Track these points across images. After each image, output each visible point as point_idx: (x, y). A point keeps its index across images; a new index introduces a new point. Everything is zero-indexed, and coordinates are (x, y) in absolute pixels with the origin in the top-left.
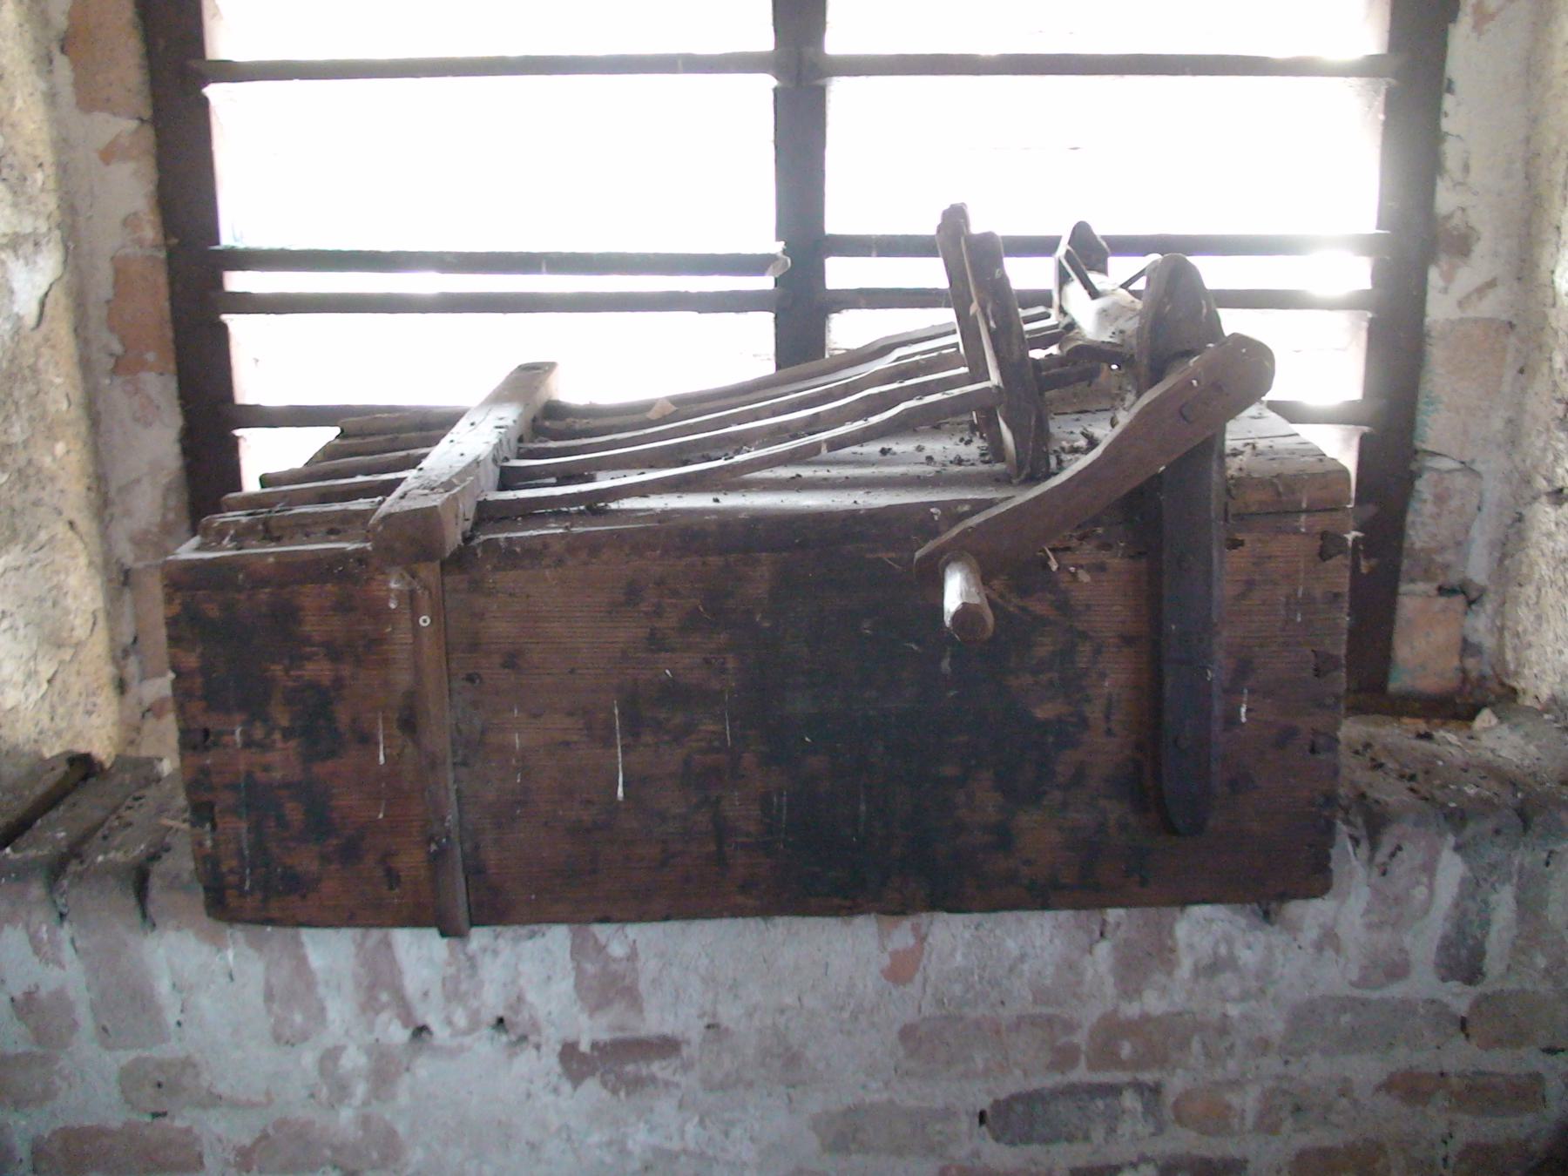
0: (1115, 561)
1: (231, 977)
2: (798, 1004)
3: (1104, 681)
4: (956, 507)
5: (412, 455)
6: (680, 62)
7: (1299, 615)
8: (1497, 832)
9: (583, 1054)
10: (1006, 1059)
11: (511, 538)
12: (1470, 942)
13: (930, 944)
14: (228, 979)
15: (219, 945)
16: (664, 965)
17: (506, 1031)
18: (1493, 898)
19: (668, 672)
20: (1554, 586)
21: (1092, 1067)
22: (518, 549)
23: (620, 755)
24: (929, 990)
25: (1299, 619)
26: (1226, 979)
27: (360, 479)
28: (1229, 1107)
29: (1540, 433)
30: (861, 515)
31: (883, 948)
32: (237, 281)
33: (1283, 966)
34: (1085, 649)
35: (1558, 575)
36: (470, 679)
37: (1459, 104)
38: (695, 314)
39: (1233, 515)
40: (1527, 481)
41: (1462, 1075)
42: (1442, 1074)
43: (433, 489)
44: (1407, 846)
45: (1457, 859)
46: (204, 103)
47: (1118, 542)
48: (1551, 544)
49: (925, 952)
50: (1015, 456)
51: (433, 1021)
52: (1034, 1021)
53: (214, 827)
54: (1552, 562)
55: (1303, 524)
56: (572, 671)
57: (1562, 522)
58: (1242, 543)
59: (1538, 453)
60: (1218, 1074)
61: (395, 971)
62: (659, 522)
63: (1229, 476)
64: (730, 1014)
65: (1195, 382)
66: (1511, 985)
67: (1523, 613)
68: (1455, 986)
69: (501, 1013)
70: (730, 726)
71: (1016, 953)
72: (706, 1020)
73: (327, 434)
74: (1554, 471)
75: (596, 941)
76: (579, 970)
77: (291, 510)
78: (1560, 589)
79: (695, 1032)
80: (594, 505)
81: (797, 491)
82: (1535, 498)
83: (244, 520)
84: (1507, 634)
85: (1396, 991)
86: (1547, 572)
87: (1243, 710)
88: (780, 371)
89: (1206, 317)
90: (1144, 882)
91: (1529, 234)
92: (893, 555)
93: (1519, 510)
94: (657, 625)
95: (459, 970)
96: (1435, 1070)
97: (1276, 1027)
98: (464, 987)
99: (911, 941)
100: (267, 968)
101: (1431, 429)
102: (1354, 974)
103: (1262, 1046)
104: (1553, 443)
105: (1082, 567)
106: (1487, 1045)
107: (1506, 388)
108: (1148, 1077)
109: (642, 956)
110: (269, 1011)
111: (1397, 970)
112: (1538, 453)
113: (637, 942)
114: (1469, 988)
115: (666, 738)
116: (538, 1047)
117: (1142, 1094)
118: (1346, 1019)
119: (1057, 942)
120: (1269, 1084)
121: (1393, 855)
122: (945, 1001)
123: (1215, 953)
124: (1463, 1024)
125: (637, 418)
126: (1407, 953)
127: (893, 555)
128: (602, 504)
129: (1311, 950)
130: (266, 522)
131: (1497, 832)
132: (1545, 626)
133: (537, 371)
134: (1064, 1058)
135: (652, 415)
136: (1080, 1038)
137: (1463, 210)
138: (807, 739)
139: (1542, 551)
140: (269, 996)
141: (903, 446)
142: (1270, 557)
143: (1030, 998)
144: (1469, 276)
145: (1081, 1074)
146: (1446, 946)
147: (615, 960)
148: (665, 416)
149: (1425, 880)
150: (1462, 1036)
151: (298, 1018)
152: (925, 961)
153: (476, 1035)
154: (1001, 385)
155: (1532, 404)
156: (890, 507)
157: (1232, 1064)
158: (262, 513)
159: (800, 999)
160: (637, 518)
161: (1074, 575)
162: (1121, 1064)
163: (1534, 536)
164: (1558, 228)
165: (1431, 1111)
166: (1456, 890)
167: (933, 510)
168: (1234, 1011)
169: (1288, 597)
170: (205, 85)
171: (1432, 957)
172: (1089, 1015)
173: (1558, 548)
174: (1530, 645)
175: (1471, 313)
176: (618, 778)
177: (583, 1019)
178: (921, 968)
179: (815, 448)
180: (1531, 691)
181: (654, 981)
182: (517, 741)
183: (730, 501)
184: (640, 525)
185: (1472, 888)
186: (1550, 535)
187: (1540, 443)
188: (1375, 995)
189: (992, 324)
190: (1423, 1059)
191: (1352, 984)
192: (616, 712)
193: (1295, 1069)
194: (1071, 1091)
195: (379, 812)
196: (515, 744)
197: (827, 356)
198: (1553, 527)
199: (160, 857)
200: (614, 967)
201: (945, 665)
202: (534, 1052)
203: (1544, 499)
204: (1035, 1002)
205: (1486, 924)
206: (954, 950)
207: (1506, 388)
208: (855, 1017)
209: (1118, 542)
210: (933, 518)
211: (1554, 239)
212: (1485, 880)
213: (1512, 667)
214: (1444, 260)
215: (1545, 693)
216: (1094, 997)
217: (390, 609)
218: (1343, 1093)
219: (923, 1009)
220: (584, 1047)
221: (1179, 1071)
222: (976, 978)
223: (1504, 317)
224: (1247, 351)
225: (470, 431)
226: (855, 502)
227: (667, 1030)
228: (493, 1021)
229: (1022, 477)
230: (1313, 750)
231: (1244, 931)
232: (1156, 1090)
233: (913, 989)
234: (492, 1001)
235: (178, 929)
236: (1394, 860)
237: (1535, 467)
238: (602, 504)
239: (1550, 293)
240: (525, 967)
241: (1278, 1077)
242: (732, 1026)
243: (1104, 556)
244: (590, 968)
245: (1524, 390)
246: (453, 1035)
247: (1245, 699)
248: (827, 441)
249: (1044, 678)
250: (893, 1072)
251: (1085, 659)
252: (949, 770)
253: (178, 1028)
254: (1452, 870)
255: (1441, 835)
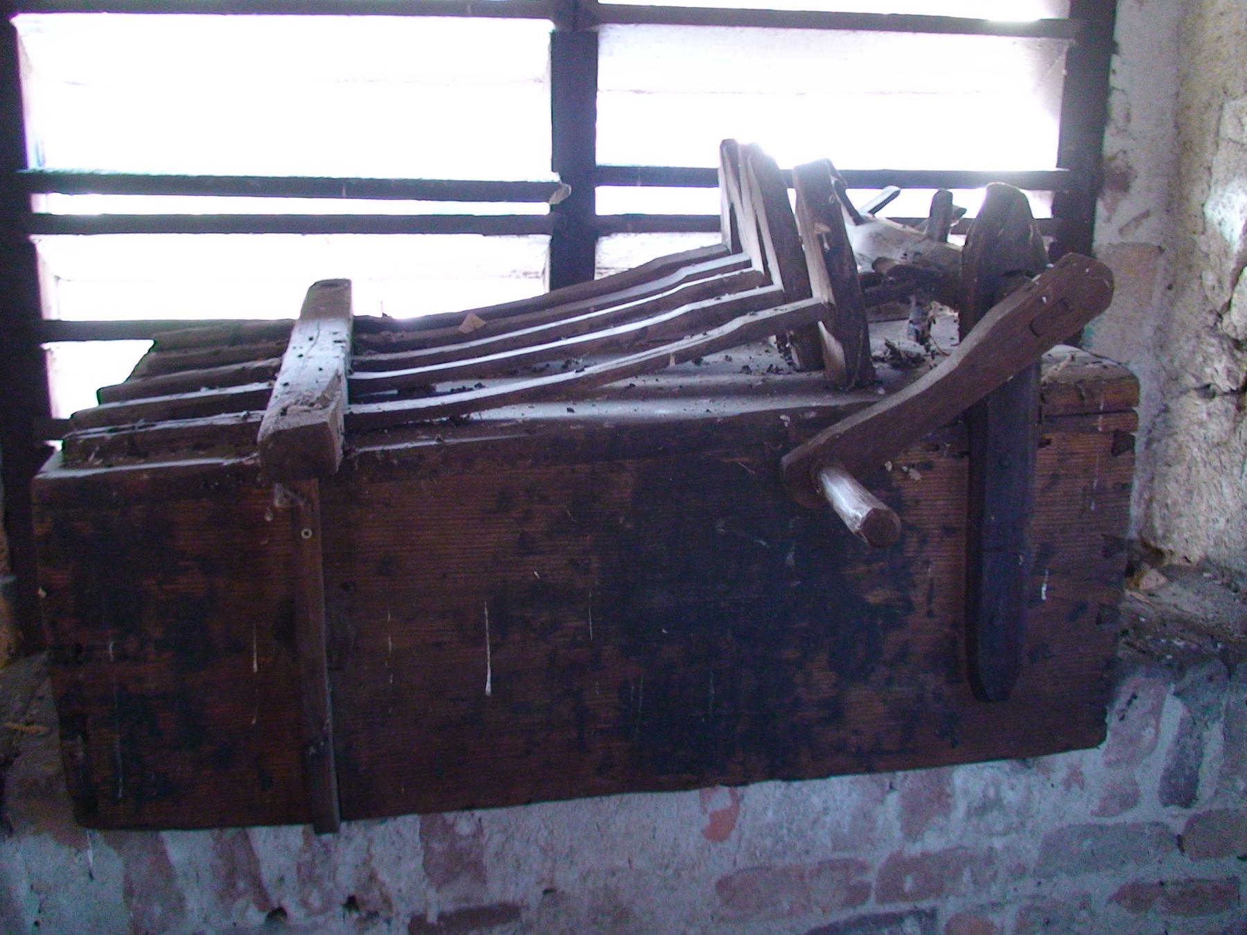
0: (942, 461)
1: (91, 876)
2: (627, 865)
3: (928, 568)
4: (803, 414)
5: (248, 368)
6: (469, 7)
7: (1093, 504)
8: (1210, 679)
9: (432, 925)
10: (809, 900)
11: (388, 451)
12: (1187, 772)
13: (745, 804)
14: (87, 878)
15: (78, 845)
16: (507, 838)
17: (357, 908)
18: (1206, 734)
19: (536, 573)
20: (1208, 466)
21: (881, 900)
22: (395, 462)
23: (489, 653)
24: (743, 845)
25: (1093, 508)
26: (993, 817)
27: (204, 392)
28: (991, 925)
29: (1188, 339)
30: (719, 423)
31: (704, 811)
32: (47, 204)
33: (1040, 803)
34: (913, 540)
35: (1212, 457)
36: (345, 587)
37: (1123, 64)
38: (479, 237)
39: (1046, 417)
40: (1175, 378)
41: (1177, 883)
42: (1162, 884)
43: (312, 405)
44: (1140, 694)
45: (1178, 703)
46: (13, 31)
47: (945, 443)
48: (1202, 431)
49: (740, 811)
50: (844, 362)
51: (290, 904)
52: (833, 865)
53: (86, 738)
54: (1204, 446)
55: (1099, 424)
56: (444, 576)
57: (1215, 413)
58: (1048, 442)
59: (1186, 355)
60: (983, 899)
61: (253, 860)
62: (528, 431)
63: (1042, 383)
64: (566, 879)
65: (1044, 299)
66: (1216, 806)
67: (1171, 487)
68: (1175, 809)
69: (352, 891)
70: (593, 621)
71: (820, 807)
72: (544, 886)
73: (141, 347)
74: (1202, 370)
75: (444, 821)
76: (427, 849)
77: (154, 426)
78: (1215, 468)
79: (534, 896)
80: (456, 416)
81: (643, 400)
82: (1185, 392)
83: (108, 436)
84: (1155, 505)
85: (1129, 817)
86: (1199, 454)
87: (1044, 589)
88: (552, 292)
89: (1033, 241)
90: (954, 744)
91: (1179, 173)
92: (747, 459)
93: (1165, 402)
94: (526, 530)
95: (314, 856)
96: (1156, 881)
97: (1031, 851)
98: (318, 871)
99: (728, 802)
100: (127, 865)
101: (1096, 336)
102: (1095, 805)
103: (1020, 871)
104: (1204, 347)
105: (913, 466)
106: (1200, 855)
107: (1155, 302)
108: (925, 905)
109: (487, 832)
110: (129, 905)
111: (1129, 800)
112: (1186, 355)
113: (483, 821)
114: (1184, 811)
115: (533, 635)
116: (388, 921)
117: (920, 920)
118: (1087, 843)
119: (854, 795)
120: (1027, 902)
121: (1129, 703)
122: (758, 854)
123: (985, 797)
124: (1180, 841)
125: (449, 331)
126: (1136, 784)
127: (747, 459)
128: (465, 416)
129: (1061, 788)
130: (131, 438)
131: (1210, 679)
132: (1196, 498)
133: (338, 289)
134: (857, 894)
135: (464, 328)
136: (871, 877)
137: (1125, 152)
138: (664, 631)
139: (1192, 436)
140: (129, 892)
141: (741, 356)
142: (1072, 454)
143: (830, 845)
144: (1128, 207)
145: (871, 907)
146: (1169, 776)
147: (461, 837)
148: (476, 330)
149: (1153, 722)
150: (1178, 851)
151: (158, 910)
152: (740, 818)
153: (329, 913)
154: (833, 301)
155: (1180, 314)
156: (742, 415)
157: (995, 889)
158: (123, 429)
159: (630, 862)
160: (502, 429)
161: (907, 473)
162: (905, 897)
163: (1183, 424)
164: (1209, 169)
165: (1151, 915)
166: (1177, 729)
167: (783, 417)
168: (998, 843)
169: (1085, 489)
170: (14, 15)
171: (1157, 786)
172: (877, 858)
173: (1210, 434)
174: (1180, 515)
175: (1129, 239)
176: (487, 674)
177: (432, 894)
178: (737, 826)
179: (664, 360)
180: (1181, 553)
181: (497, 854)
182: (390, 644)
183: (584, 411)
184: (507, 437)
185: (1190, 728)
186: (1201, 424)
187: (1188, 347)
188: (1110, 821)
189: (826, 246)
190: (1148, 873)
191: (1092, 813)
192: (486, 613)
193: (1046, 889)
194: (862, 922)
195: (252, 717)
196: (388, 646)
197: (597, 277)
198: (1204, 416)
199: (11, 763)
200: (462, 844)
201: (790, 558)
202: (385, 926)
203: (1193, 394)
204: (835, 848)
205: (1200, 755)
206: (766, 808)
207: (1155, 302)
208: (677, 873)
209: (945, 443)
210: (784, 424)
211: (1205, 177)
212: (1200, 720)
213: (1160, 532)
214: (1108, 195)
215: (1196, 554)
216: (885, 840)
217: (267, 522)
218: (1083, 906)
219: (738, 861)
220: (432, 918)
221: (952, 898)
222: (785, 831)
223: (1155, 243)
224: (1084, 271)
225: (312, 346)
226: (708, 411)
227: (509, 898)
228: (344, 901)
229: (853, 385)
230: (1099, 621)
231: (1009, 775)
232: (932, 915)
233: (730, 845)
234: (346, 880)
235: (36, 833)
236: (1131, 707)
237: (1183, 367)
238: (465, 416)
239: (1200, 222)
240: (377, 850)
241: (1034, 897)
242: (568, 890)
243: (932, 456)
244: (437, 846)
245: (1172, 303)
246: (308, 915)
247: (1046, 580)
248: (675, 354)
249: (875, 567)
250: (710, 920)
251: (912, 549)
252: (791, 654)
253: (36, 928)
254: (1174, 711)
255: (1167, 683)
